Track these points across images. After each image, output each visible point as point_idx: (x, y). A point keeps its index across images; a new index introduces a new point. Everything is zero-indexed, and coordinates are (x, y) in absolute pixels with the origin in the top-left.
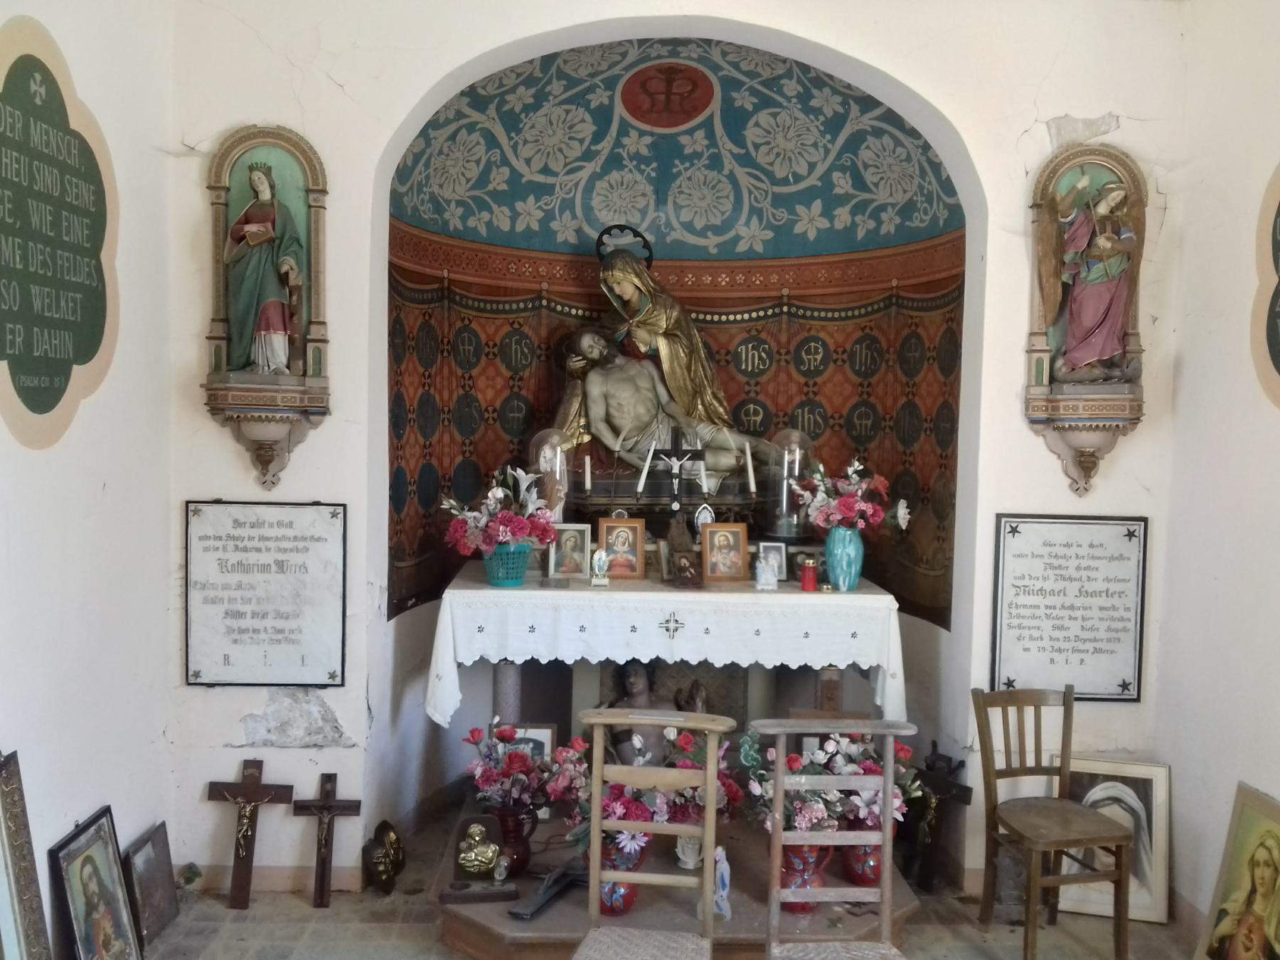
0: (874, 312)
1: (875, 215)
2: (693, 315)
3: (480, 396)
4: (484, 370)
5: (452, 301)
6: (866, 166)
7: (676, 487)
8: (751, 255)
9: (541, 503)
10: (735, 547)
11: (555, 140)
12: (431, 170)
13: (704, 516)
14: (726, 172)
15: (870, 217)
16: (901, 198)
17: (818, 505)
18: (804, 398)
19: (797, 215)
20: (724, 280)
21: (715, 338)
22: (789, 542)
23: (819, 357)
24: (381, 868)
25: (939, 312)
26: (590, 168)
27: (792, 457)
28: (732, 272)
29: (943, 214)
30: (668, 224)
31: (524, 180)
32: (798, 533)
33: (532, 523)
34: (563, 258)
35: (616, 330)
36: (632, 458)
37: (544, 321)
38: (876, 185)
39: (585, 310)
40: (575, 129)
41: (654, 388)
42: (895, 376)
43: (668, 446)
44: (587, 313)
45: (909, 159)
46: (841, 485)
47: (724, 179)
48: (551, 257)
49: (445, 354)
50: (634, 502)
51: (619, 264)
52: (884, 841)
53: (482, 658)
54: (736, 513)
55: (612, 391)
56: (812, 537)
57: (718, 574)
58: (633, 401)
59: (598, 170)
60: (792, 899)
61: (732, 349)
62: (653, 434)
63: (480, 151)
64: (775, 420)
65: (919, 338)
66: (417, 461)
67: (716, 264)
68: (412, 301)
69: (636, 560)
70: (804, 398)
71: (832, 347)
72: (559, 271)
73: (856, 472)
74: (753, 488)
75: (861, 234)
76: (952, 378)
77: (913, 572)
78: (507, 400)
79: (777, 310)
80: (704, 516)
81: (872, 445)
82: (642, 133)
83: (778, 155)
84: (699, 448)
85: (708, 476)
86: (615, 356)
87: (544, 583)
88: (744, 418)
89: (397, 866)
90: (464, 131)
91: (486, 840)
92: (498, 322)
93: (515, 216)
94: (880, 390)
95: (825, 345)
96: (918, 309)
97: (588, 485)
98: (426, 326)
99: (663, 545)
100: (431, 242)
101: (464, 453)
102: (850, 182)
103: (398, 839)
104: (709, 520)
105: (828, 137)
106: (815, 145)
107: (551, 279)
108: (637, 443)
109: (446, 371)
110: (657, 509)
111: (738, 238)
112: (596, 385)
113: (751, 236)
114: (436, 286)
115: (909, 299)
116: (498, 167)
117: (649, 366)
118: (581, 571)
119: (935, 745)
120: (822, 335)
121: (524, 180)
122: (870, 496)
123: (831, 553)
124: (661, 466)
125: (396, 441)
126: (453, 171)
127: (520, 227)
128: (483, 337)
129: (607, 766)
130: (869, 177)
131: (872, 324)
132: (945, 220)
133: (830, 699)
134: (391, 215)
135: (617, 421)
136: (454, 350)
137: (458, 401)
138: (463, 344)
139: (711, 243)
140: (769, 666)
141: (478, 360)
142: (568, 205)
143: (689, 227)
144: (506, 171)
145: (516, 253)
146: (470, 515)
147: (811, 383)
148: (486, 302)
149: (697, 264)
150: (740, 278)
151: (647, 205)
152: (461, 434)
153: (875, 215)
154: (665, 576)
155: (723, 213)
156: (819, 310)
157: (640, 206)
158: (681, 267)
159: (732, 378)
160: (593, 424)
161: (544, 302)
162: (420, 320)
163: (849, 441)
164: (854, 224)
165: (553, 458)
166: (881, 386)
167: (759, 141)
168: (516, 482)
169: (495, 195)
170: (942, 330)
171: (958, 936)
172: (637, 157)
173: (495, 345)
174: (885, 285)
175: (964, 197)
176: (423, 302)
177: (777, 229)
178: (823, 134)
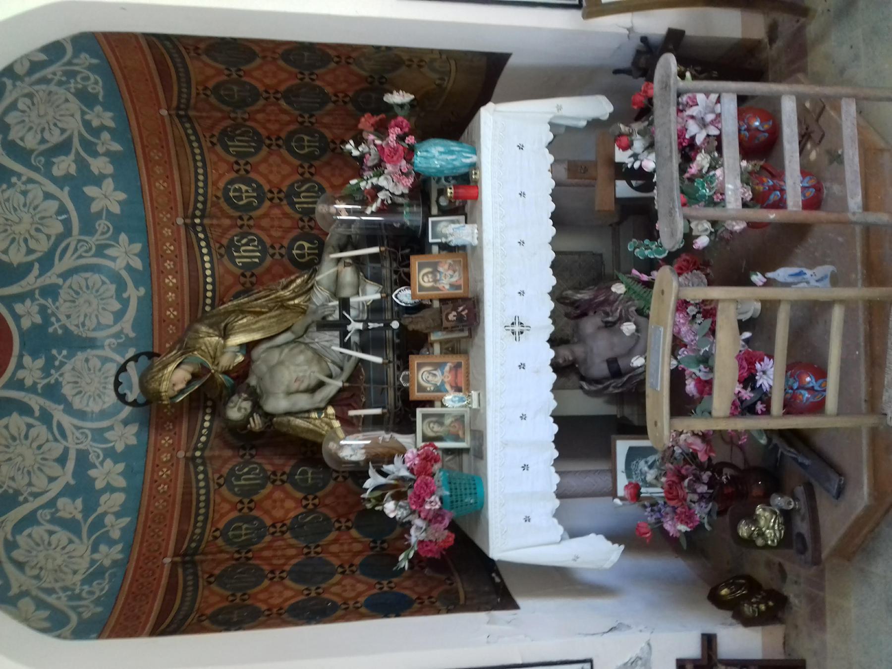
0: (195, 133)
1: (96, 132)
2: (208, 308)
3: (292, 514)
4: (267, 512)
5: (195, 551)
6: (43, 141)
7: (376, 325)
8: (144, 255)
9: (397, 460)
10: (435, 266)
11: (28, 453)
12: (57, 586)
13: (404, 296)
14: (60, 281)
15: (99, 138)
16: (75, 105)
17: (392, 184)
18: (285, 202)
19: (102, 210)
20: (171, 281)
21: (229, 288)
22: (427, 214)
23: (244, 188)
24: (763, 607)
25: (190, 67)
26: (59, 414)
27: (344, 212)
28: (162, 272)
29: (85, 59)
30: (117, 336)
31: (72, 482)
32: (418, 205)
33: (419, 474)
34: (153, 438)
35: (223, 385)
36: (349, 367)
37: (217, 453)
38: (63, 131)
39: (205, 414)
40: (16, 434)
41: (278, 346)
42: (258, 111)
43: (337, 333)
44: (208, 411)
45: (30, 96)
46: (370, 161)
47: (68, 282)
48: (151, 449)
49: (250, 555)
50: (391, 365)
51: (154, 385)
52: (791, 93)
53: (555, 516)
54: (400, 263)
55: (283, 388)
56: (422, 190)
57: (461, 282)
58: (292, 368)
59: (62, 407)
60: (859, 199)
61: (238, 272)
62: (324, 347)
63: (38, 532)
64: (307, 230)
65: (217, 88)
66: (359, 581)
67: (155, 288)
68: (194, 600)
69: (450, 361)
70: (285, 202)
71: (233, 175)
72: (166, 441)
73: (357, 147)
74: (375, 250)
75: (116, 147)
76: (256, 49)
77: (452, 90)
78: (295, 485)
79: (199, 229)
80: (404, 296)
81: (329, 135)
82: (20, 366)
83: (38, 230)
84: (336, 303)
85: (364, 293)
86: (249, 386)
87: (479, 452)
88: (307, 258)
89: (753, 586)
90: (15, 554)
91: (753, 519)
92: (218, 500)
93: (110, 488)
94: (273, 127)
95: (232, 182)
96: (189, 88)
97: (378, 411)
98: (221, 580)
99: (434, 337)
100: (134, 580)
101: (348, 528)
102: (63, 158)
103: (726, 586)
104: (408, 292)
105: (14, 180)
106: (25, 193)
107: (174, 448)
108: (334, 362)
109: (266, 553)
110: (397, 341)
111: (129, 268)
112: (277, 404)
113: (125, 254)
114: (180, 571)
115: (179, 97)
116: (57, 511)
117: (257, 353)
118: (463, 416)
119: (617, 72)
120: (221, 185)
121: (72, 482)
122: (381, 130)
123: (440, 171)
124: (356, 339)
125: (340, 613)
126: (59, 561)
127: (121, 482)
128: (234, 514)
129: (714, 413)
130: (55, 138)
131: (208, 135)
132: (92, 57)
133: (586, 170)
134: (99, 636)
135: (313, 382)
136: (246, 545)
137: (296, 537)
138: (241, 536)
139: (134, 294)
140: (553, 231)
141: (256, 518)
142: (99, 435)
143: (119, 316)
144: (61, 502)
145: (147, 486)
146: (415, 536)
147: (269, 195)
148: (197, 515)
149: (156, 306)
150: (169, 265)
151: (98, 357)
152: (330, 531)
153: (96, 132)
154: (466, 334)
155: (103, 283)
156: (197, 187)
157: (98, 364)
158: (160, 321)
159: (268, 270)
160: (317, 405)
161: (198, 454)
162: (214, 587)
163: (325, 158)
164: (108, 153)
165: (352, 447)
166: (269, 126)
167: (24, 249)
168: (377, 488)
169: (88, 510)
170: (208, 61)
171: (822, 37)
172: (46, 370)
173: (241, 502)
174: (167, 120)
175: (61, 31)
176: (196, 586)
177: (118, 230)
178: (11, 185)
